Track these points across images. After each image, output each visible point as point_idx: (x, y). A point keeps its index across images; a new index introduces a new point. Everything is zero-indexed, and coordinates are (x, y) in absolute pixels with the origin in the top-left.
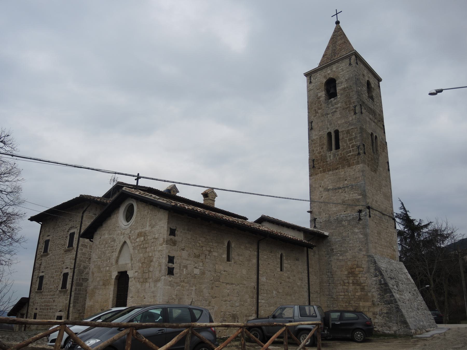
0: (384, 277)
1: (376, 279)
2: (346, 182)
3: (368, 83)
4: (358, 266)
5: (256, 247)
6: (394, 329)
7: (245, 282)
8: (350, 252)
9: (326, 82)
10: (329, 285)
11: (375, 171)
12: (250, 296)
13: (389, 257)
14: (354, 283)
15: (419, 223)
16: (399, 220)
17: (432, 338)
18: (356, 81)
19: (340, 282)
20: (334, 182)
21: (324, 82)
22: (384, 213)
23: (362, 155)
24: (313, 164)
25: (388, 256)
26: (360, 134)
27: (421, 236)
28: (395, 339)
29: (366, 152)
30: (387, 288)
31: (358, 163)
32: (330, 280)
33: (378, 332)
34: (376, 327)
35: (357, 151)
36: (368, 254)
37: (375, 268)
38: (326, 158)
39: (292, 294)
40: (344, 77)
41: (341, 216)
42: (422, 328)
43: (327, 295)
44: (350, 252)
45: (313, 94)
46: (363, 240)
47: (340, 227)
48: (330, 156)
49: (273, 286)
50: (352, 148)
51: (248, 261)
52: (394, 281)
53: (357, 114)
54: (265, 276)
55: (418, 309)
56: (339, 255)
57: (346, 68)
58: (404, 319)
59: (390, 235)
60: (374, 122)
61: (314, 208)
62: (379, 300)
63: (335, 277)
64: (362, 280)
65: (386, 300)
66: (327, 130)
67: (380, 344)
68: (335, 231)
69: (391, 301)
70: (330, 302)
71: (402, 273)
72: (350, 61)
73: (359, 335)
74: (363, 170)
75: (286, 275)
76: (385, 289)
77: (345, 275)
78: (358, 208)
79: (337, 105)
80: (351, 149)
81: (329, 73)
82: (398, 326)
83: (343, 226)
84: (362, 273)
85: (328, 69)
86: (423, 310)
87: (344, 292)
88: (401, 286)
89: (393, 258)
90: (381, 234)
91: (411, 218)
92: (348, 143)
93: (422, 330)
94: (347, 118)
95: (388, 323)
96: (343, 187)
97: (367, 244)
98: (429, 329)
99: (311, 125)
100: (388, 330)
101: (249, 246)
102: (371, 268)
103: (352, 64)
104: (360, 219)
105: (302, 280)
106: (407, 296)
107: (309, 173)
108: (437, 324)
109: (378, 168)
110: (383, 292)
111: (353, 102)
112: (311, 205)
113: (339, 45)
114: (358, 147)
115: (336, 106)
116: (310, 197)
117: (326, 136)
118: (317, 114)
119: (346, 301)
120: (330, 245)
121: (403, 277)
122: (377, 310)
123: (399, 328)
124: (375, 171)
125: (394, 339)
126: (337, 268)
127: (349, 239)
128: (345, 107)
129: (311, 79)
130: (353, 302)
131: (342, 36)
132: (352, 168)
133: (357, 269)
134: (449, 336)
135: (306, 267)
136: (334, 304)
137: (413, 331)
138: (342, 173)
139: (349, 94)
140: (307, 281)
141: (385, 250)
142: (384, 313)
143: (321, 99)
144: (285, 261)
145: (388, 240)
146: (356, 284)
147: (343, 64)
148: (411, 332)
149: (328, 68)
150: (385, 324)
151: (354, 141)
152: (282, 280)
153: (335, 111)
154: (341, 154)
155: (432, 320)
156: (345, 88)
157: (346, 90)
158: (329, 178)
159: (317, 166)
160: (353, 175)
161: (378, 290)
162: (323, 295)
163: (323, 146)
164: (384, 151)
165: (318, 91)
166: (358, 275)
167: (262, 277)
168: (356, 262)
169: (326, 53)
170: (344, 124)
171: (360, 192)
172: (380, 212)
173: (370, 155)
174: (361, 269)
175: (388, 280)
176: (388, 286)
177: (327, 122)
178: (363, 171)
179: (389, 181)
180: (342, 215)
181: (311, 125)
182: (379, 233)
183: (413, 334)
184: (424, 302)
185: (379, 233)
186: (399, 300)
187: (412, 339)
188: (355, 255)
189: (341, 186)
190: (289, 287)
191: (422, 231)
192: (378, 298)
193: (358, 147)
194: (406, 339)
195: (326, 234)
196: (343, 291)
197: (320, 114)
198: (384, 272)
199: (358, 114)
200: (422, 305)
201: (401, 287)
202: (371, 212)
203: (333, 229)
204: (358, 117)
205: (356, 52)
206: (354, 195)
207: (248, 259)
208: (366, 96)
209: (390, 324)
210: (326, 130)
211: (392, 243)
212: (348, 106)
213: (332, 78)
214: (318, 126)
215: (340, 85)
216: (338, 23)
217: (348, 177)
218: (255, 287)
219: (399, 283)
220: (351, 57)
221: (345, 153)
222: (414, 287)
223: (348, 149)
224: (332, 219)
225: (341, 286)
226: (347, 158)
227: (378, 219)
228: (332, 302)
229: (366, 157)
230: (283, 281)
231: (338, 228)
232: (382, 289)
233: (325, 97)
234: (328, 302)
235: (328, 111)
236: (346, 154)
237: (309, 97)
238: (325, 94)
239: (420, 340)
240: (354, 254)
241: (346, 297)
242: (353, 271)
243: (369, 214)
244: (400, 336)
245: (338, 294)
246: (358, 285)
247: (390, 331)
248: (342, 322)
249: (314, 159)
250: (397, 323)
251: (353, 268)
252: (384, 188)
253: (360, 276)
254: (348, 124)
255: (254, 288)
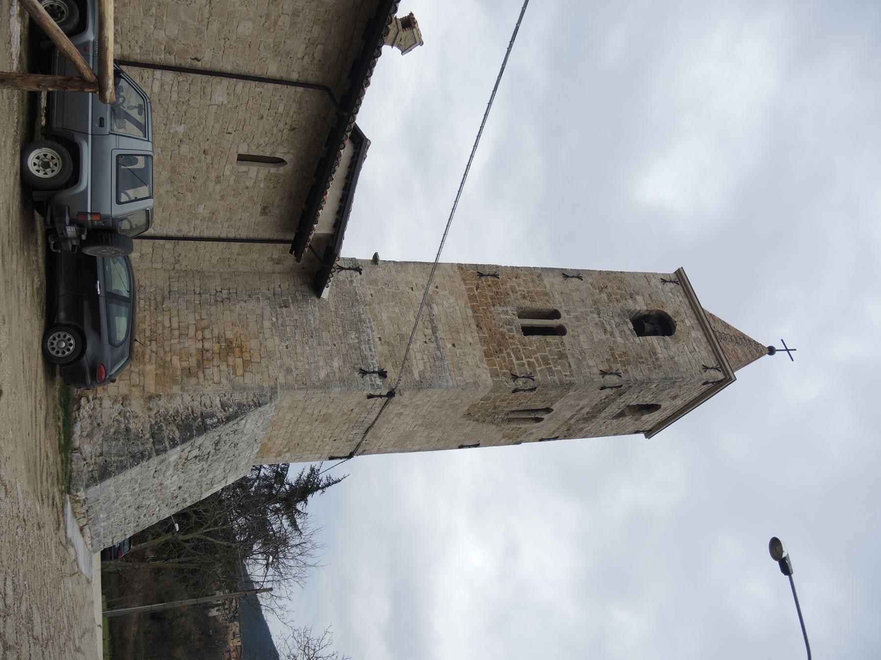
0: (222, 425)
1: (216, 406)
2: (449, 346)
3: (651, 408)
4: (246, 363)
5: (311, 79)
6: (85, 447)
7: (215, 26)
8: (283, 346)
9: (666, 314)
10: (195, 293)
11: (468, 415)
12: (174, 40)
13: (266, 441)
14: (204, 352)
15: (300, 511)
16: (306, 475)
17: (64, 542)
18: (672, 378)
19: (206, 319)
20: (449, 317)
21: (666, 311)
22: (370, 433)
23: (512, 385)
24: (488, 275)
25: (269, 439)
26: (558, 383)
27: (275, 515)
28: (57, 447)
29: (517, 394)
30: (195, 431)
31: (494, 374)
32: (208, 296)
33: (76, 406)
34: (88, 401)
35: (522, 373)
36: (279, 388)
37: (245, 403)
38: (502, 304)
39: (175, 187)
40: (678, 352)
41: (369, 330)
42: (89, 518)
43: (170, 285)
44: (283, 346)
45: (639, 285)
46: (314, 378)
47: (344, 327)
48: (506, 313)
49: (198, 127)
50: (526, 364)
51: (276, 47)
52: (210, 451)
53: (603, 377)
54: (229, 102)
55: (138, 507)
56: (274, 319)
57: (698, 360)
58: (114, 472)
59: (317, 446)
60: (570, 419)
61: (385, 269)
62: (162, 410)
63: (217, 307)
64: (212, 371)
65: (162, 427)
66: (565, 310)
67: (40, 401)
68: (333, 313)
69: (161, 442)
70: (151, 292)
71: (228, 471)
72: (712, 368)
73: (65, 344)
74: (479, 385)
75: (227, 173)
76: (191, 426)
77: (224, 333)
78: (389, 368)
79: (619, 336)
80: (525, 361)
81: (685, 322)
82: (94, 457)
83: (346, 334)
84: (229, 373)
85: (692, 322)
86: (135, 519)
87: (179, 329)
88: (195, 467)
89: (263, 451)
90: (324, 424)
91: (309, 498)
92: (538, 355)
93: (84, 517)
94: (593, 356)
95: (102, 432)
96: (436, 337)
97: (303, 386)
98: (89, 535)
99: (575, 275)
100: (82, 432)
101: (315, 55)
102: (245, 394)
103: (705, 372)
104: (364, 373)
105: (210, 220)
106: (172, 481)
107: (466, 264)
108: (101, 552)
109: (474, 421)
110: (183, 421)
111: (626, 371)
112: (393, 264)
113: (734, 350)
114: (530, 377)
115: (617, 334)
116: (410, 262)
117: (551, 306)
118: (597, 291)
119: (155, 332)
120: (297, 301)
121: (218, 472)
122: (136, 406)
123: (88, 460)
124: (468, 415)
125: (58, 444)
126: (240, 315)
127: (314, 345)
128: (617, 353)
129: (671, 283)
130: (154, 349)
131: (749, 356)
132: (481, 361)
133: (239, 361)
134: (70, 586)
135: (244, 235)
136: (148, 303)
137: (81, 495)
138: (471, 336)
139: (643, 362)
140: (206, 234)
141: (283, 431)
142: (129, 423)
143: (630, 301)
144: (264, 171)
145: (306, 440)
146: (200, 357)
147: (706, 353)
148: (80, 491)
149: (696, 322)
150: (99, 425)
151: (544, 367)
152: (213, 159)
153: (605, 330)
154: (512, 338)
155: (111, 540)
156: (655, 353)
157: (651, 357)
158: (457, 308)
159: (483, 282)
160: (467, 362)
161: (188, 410)
162: (170, 278)
163: (529, 298)
164: (504, 437)
165: (648, 297)
166: (225, 363)
167: (226, 93)
168: (259, 360)
169: (718, 321)
170: (579, 348)
171: (427, 376)
172: (374, 422)
173: (506, 403)
174: (240, 372)
175: (213, 435)
176: (199, 434)
177: (582, 310)
178: (475, 384)
179: (438, 447)
180: (372, 332)
181: (573, 277)
182: (326, 419)
183: (75, 494)
184: (155, 520)
185: (326, 419)
186: (163, 461)
187: (59, 491)
188: (275, 358)
189: (440, 334)
190: (194, 178)
191: (285, 517)
192: (166, 409)
193: (530, 377)
194: (58, 476)
195: (326, 293)
196: (181, 325)
197: (597, 296)
198: (235, 426)
199: (602, 379)
200: (147, 516)
201: (194, 467)
202: (380, 399)
203: (337, 309)
204: (595, 380)
205: (731, 381)
206: (421, 363)
207: (282, 46)
208: (631, 400)
209: (98, 438)
210: (564, 308)
211: (297, 451)
212: (619, 359)
213: (675, 328)
214: (572, 291)
215: (662, 344)
216: (771, 351)
217: (461, 350)
218: (199, 60)
219: (204, 463)
220: (720, 371)
221: (515, 347)
222: (193, 498)
223: (525, 355)
224: (361, 308)
225: (195, 322)
226: (504, 351)
227: (360, 417)
228: (152, 298)
229: (505, 394)
230: (211, 162)
231: (339, 322)
232: (190, 419)
233: (635, 310)
234: (152, 287)
235: (606, 314)
236: (513, 349)
237: (633, 275)
238: (641, 312)
239: (58, 511)
240: (278, 355)
241: (167, 331)
242: (234, 352)
243: (375, 394)
244: (66, 461)
245: (175, 313)
246: (198, 361)
247: (81, 436)
248: (102, 302)
249: (498, 278)
250: (101, 454)
251: (242, 352)
252: (426, 434)
253: (224, 367)
254: (580, 358)
255: (197, 59)
